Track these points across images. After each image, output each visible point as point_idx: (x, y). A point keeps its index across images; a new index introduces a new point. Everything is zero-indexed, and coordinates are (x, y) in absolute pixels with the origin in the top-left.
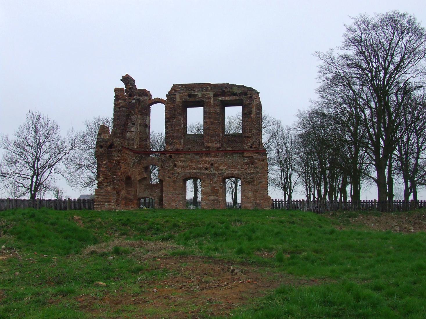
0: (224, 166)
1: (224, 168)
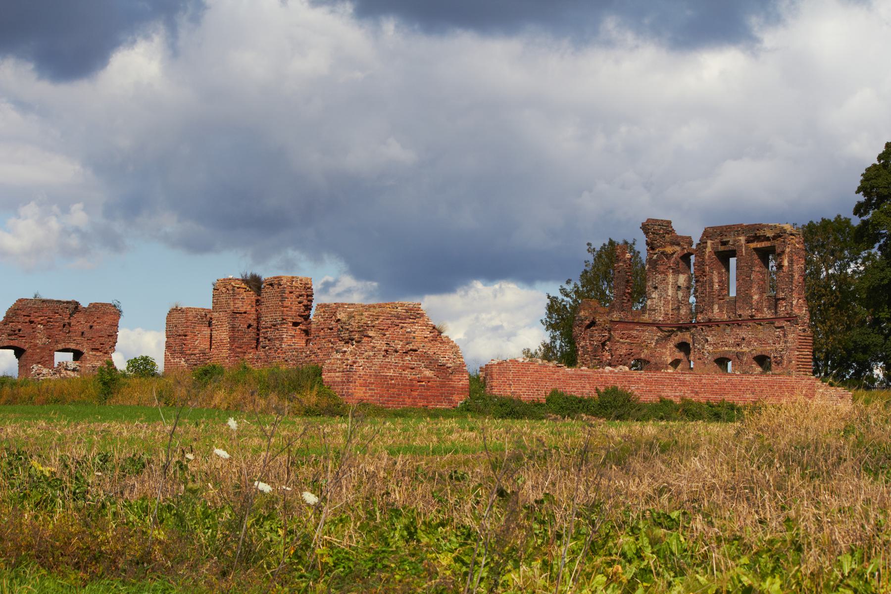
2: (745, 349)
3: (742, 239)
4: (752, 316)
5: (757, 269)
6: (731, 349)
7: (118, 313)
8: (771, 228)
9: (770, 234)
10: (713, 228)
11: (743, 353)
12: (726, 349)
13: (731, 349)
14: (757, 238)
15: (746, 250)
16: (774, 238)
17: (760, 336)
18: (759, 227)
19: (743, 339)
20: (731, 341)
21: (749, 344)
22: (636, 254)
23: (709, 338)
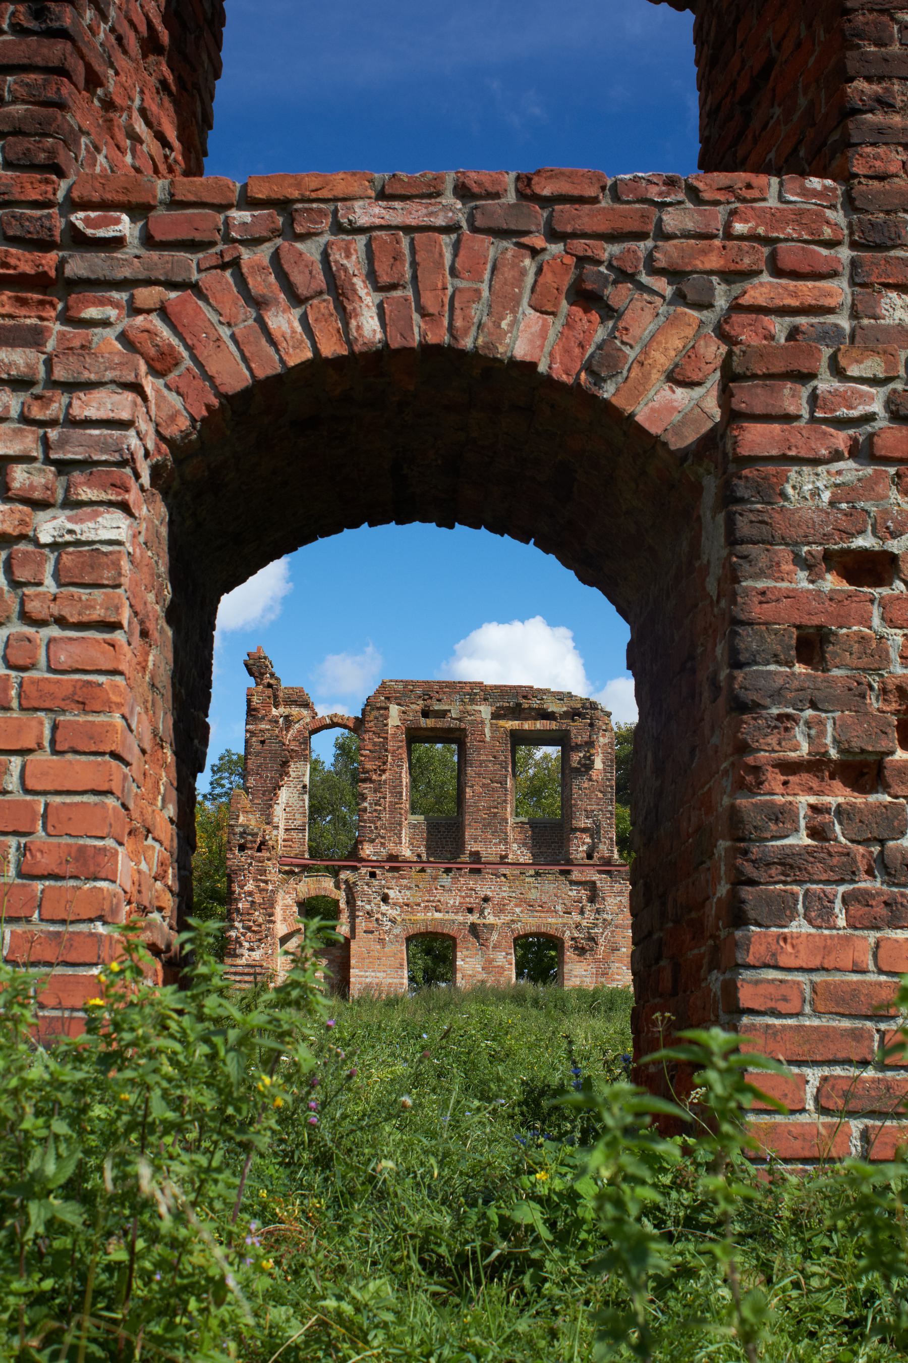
0: (516, 906)
1: (518, 910)
2: (491, 919)
3: (485, 711)
4: (503, 857)
5: (144, 866)
6: (451, 916)
7: (701, 167)
8: (561, 697)
9: (553, 707)
10: (406, 683)
11: (491, 927)
12: (438, 915)
13: (451, 916)
14: (517, 712)
15: (492, 731)
16: (565, 715)
17: (533, 895)
18: (527, 692)
19: (486, 899)
20: (453, 900)
21: (501, 909)
22: (761, 574)
23: (391, 893)
